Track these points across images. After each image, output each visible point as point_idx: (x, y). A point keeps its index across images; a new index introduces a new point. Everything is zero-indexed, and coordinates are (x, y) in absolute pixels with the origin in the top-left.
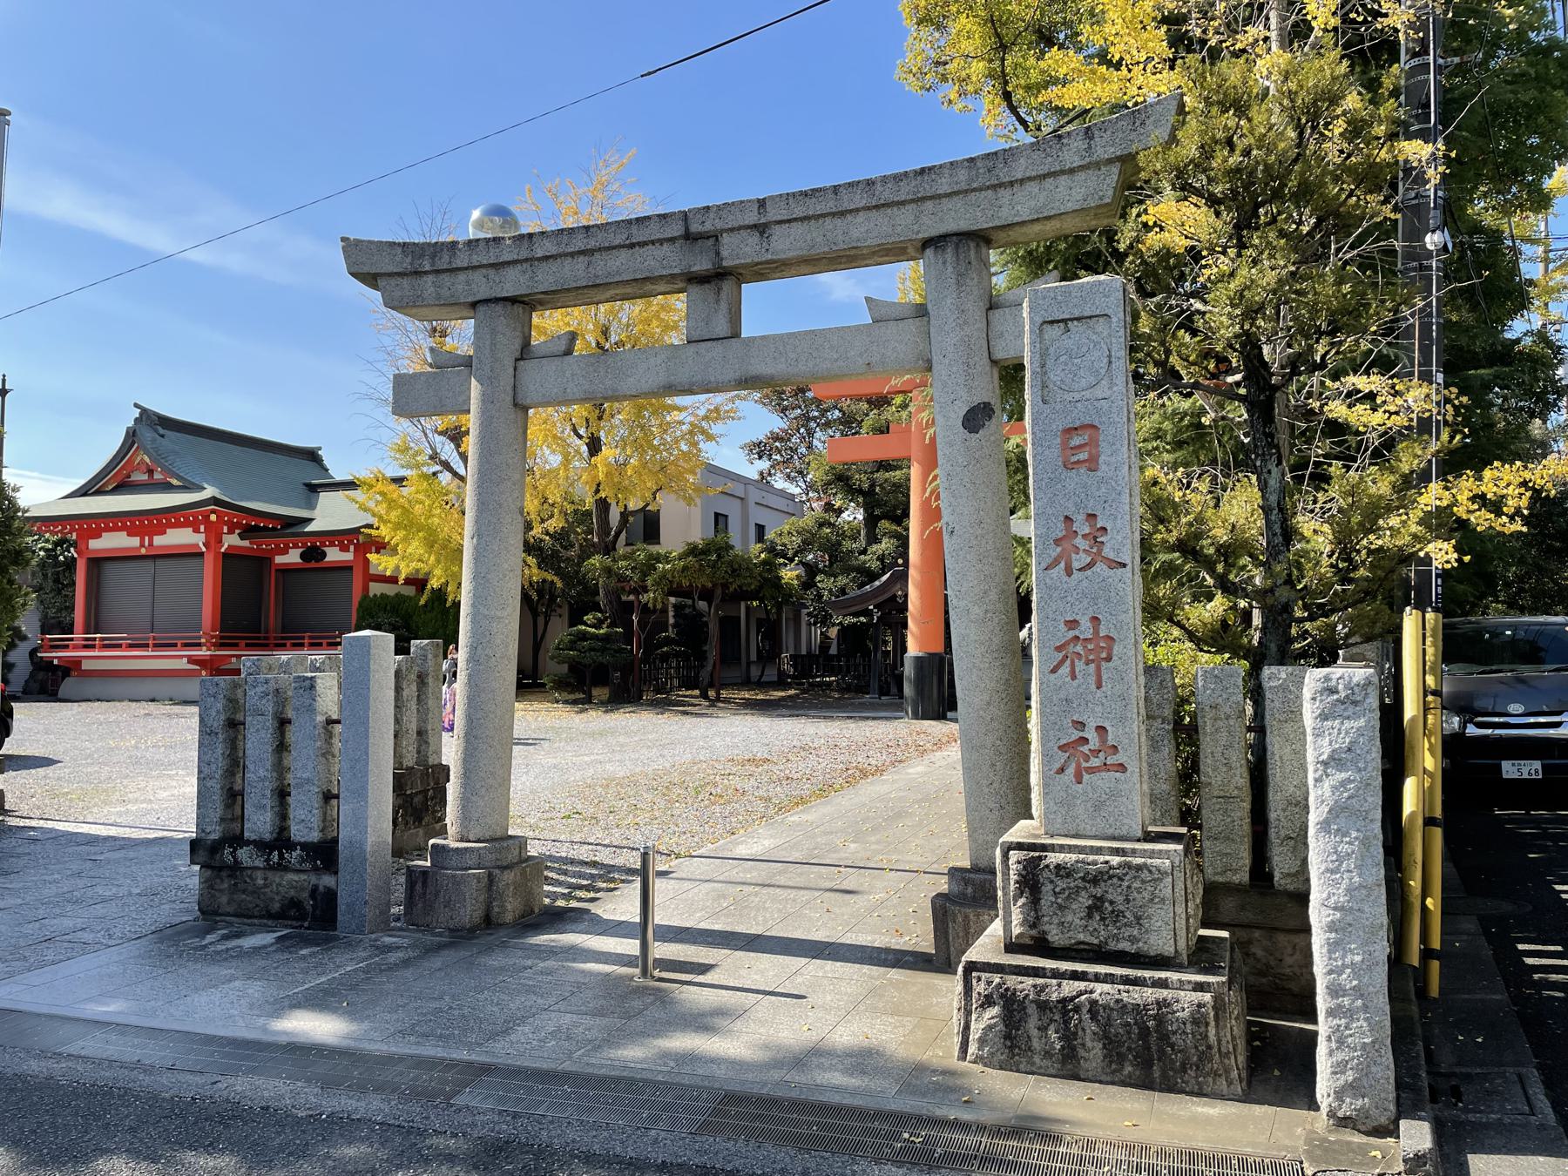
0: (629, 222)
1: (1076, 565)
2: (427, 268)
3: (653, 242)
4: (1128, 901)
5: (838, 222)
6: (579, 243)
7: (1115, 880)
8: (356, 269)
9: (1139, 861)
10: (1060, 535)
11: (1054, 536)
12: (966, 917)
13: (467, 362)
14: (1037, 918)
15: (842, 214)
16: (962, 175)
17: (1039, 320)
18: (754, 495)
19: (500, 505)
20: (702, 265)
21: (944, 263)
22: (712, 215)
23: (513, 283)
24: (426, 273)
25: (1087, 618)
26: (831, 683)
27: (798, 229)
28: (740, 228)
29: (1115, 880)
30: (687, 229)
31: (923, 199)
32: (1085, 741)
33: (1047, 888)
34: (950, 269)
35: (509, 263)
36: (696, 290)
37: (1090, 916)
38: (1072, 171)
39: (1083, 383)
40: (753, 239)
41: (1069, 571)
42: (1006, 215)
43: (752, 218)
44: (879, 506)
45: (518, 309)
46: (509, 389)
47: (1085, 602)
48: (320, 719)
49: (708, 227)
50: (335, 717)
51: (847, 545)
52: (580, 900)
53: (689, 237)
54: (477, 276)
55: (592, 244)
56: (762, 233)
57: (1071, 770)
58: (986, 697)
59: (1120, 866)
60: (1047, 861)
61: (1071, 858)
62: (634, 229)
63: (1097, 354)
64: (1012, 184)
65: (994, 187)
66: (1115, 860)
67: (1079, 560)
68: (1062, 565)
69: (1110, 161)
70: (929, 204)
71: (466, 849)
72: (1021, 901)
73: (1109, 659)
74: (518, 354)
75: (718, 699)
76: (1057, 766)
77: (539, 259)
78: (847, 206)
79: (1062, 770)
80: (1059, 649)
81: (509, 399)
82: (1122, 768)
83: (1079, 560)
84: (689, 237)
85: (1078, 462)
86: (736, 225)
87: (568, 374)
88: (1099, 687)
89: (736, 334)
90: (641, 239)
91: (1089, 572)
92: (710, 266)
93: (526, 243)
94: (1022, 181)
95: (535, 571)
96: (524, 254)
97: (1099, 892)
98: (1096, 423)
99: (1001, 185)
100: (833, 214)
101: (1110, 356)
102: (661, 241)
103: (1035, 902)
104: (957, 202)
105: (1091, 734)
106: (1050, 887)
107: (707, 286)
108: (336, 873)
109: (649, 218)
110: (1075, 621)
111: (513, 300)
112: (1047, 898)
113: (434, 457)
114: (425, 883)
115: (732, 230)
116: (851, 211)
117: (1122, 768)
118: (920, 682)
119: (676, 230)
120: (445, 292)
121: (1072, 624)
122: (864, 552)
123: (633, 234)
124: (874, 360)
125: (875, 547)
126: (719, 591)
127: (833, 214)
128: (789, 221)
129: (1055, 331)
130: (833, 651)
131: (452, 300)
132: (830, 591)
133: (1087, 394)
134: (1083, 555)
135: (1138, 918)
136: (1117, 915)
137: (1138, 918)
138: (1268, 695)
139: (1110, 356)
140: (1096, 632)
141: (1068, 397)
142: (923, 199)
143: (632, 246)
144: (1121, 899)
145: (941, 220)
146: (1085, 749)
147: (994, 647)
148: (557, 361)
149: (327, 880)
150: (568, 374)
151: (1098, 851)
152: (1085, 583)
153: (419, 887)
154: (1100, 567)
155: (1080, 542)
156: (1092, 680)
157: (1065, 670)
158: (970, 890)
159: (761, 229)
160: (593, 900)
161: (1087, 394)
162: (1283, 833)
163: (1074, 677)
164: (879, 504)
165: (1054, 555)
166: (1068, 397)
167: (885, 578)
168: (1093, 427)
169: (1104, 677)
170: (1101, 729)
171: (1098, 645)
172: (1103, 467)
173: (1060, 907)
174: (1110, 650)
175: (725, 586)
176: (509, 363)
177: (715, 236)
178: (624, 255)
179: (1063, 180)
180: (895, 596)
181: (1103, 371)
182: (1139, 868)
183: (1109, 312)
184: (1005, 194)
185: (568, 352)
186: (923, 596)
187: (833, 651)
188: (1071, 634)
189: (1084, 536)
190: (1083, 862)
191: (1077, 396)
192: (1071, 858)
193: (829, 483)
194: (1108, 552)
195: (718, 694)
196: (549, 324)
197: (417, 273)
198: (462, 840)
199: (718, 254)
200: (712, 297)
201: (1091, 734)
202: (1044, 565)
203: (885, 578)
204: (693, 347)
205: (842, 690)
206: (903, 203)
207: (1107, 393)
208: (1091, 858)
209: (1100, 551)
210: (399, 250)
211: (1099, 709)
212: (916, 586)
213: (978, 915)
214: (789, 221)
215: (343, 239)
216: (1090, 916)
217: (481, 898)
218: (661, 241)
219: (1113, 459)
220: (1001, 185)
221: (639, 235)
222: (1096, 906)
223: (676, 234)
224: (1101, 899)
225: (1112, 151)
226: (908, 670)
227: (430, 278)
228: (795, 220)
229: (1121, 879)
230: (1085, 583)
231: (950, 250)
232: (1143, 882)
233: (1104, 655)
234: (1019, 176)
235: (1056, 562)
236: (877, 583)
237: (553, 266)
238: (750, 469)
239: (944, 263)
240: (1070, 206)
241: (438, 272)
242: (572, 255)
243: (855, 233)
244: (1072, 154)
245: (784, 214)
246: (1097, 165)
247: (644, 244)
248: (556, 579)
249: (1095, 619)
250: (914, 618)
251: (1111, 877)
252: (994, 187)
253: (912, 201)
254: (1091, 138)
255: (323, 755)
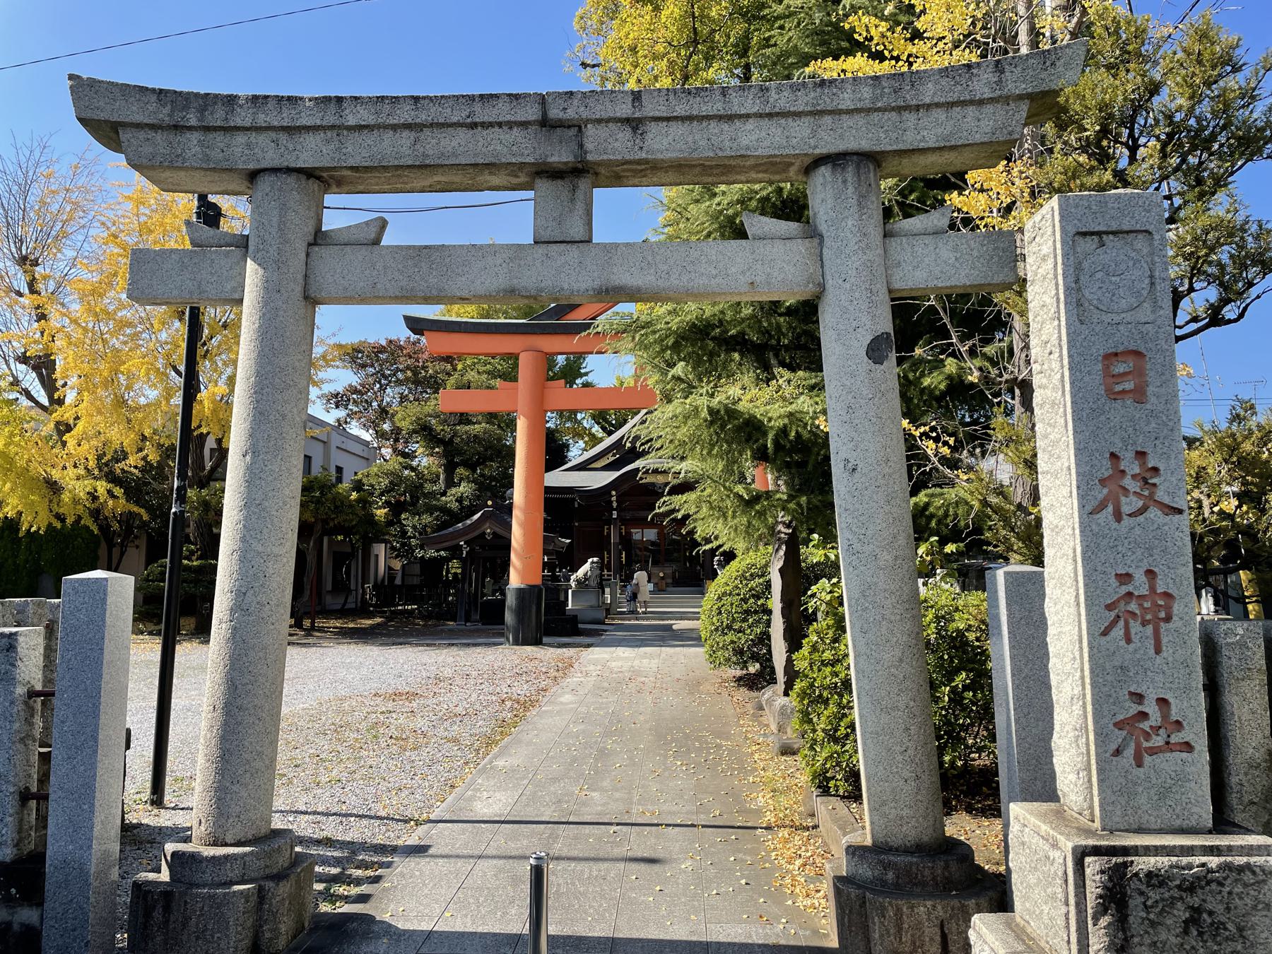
0: (472, 98)
1: (1126, 509)
2: (193, 122)
3: (500, 125)
4: (1228, 909)
5: (725, 127)
6: (405, 114)
7: (1214, 886)
8: (83, 115)
9: (1241, 860)
10: (1106, 474)
11: (1099, 475)
12: (898, 911)
13: (242, 243)
14: (1126, 940)
15: (730, 118)
16: (866, 92)
17: (1072, 230)
18: (336, 440)
19: (284, 417)
20: (561, 155)
21: (845, 182)
22: (575, 102)
23: (311, 151)
24: (190, 128)
25: (1142, 571)
26: (413, 610)
27: (677, 129)
28: (608, 120)
29: (1214, 886)
30: (545, 114)
31: (822, 113)
32: (1144, 716)
33: (1135, 902)
34: (851, 189)
35: (308, 129)
36: (543, 185)
37: (1186, 932)
38: (981, 102)
39: (1123, 304)
40: (624, 134)
41: (1118, 516)
42: (910, 140)
43: (625, 110)
44: (460, 454)
45: (314, 185)
46: (300, 277)
47: (1139, 552)
48: (20, 690)
49: (571, 114)
50: (39, 687)
51: (428, 487)
52: (347, 899)
53: (546, 123)
54: (263, 139)
55: (423, 117)
56: (635, 129)
57: (1130, 752)
58: (898, 653)
59: (1221, 867)
60: (1135, 869)
61: (1163, 862)
62: (477, 107)
63: (1137, 273)
64: (918, 108)
65: (899, 109)
66: (1213, 862)
67: (1135, 503)
68: (1110, 508)
69: (1020, 97)
70: (827, 120)
71: (226, 857)
72: (1105, 921)
73: (1168, 619)
74: (311, 238)
75: (313, 628)
76: (1114, 747)
77: (350, 128)
78: (736, 109)
79: (1117, 752)
80: (1109, 607)
81: (299, 289)
82: (1188, 747)
83: (1130, 504)
84: (546, 123)
85: (1124, 392)
86: (605, 115)
87: (379, 266)
88: (1158, 650)
89: (590, 241)
90: (486, 119)
91: (1141, 518)
92: (571, 159)
93: (333, 107)
94: (928, 107)
95: (122, 501)
96: (331, 119)
97: (1195, 901)
98: (1142, 349)
99: (907, 108)
100: (720, 118)
101: (1151, 277)
102: (511, 125)
103: (1121, 922)
104: (859, 120)
105: (1151, 708)
106: (1141, 899)
107: (560, 182)
108: (40, 904)
109: (496, 96)
110: (1128, 575)
111: (309, 174)
112: (1136, 915)
113: (16, 382)
114: (167, 909)
115: (599, 121)
116: (740, 116)
117: (1188, 747)
118: (521, 611)
119: (532, 113)
120: (216, 154)
121: (1125, 578)
122: (444, 494)
123: (475, 112)
124: (758, 279)
125: (454, 490)
126: (319, 527)
127: (720, 118)
128: (668, 119)
129: (1089, 244)
130: (398, 581)
131: (225, 165)
132: (414, 527)
133: (1128, 317)
134: (1134, 499)
135: (1241, 930)
136: (1219, 927)
137: (1241, 930)
138: (1225, 652)
139: (1151, 277)
140: (1152, 589)
141: (1107, 318)
142: (822, 113)
143: (473, 126)
144: (1220, 908)
145: (841, 136)
146: (1145, 725)
147: (905, 597)
148: (364, 251)
149: (27, 915)
150: (379, 266)
151: (1190, 851)
152: (1138, 531)
153: (158, 914)
154: (1154, 513)
155: (1128, 482)
156: (1150, 644)
157: (1118, 632)
158: (890, 876)
159: (634, 124)
160: (363, 898)
161: (1128, 317)
162: (1246, 799)
163: (1128, 640)
164: (460, 452)
165: (1100, 497)
166: (1107, 318)
167: (476, 517)
168: (1137, 354)
169: (1164, 640)
170: (1163, 702)
171: (1155, 604)
172: (1153, 399)
173: (1153, 924)
174: (1169, 609)
175: (325, 522)
176: (301, 247)
177: (578, 127)
178: (463, 134)
179: (971, 111)
180: (484, 533)
181: (1145, 293)
182: (1241, 869)
183: (1151, 228)
184: (910, 118)
185: (376, 242)
186: (526, 534)
187: (398, 581)
188: (1124, 590)
189: (1134, 477)
190: (1177, 867)
191: (1117, 318)
192: (1163, 862)
193: (415, 432)
194: (1161, 495)
195: (313, 623)
196: (342, 211)
197: (177, 128)
198: (215, 844)
199: (581, 146)
200: (565, 194)
201: (1151, 708)
202: (1089, 508)
203: (476, 517)
204: (542, 249)
205: (427, 617)
206: (797, 115)
207: (1151, 318)
208: (1185, 860)
209: (1151, 496)
210: (154, 98)
211: (1160, 678)
212: (520, 525)
213: (912, 908)
214: (668, 119)
215: (71, 77)
216: (1186, 932)
217: (249, 923)
218: (511, 125)
219: (1163, 390)
220: (907, 108)
221: (483, 114)
222: (1194, 919)
223: (531, 118)
224: (1196, 911)
225: (1022, 88)
226: (511, 600)
227: (194, 137)
228: (676, 118)
229: (1221, 884)
230: (1138, 531)
231: (850, 169)
232: (1246, 885)
233: (1162, 615)
234: (927, 100)
235: (1101, 507)
236: (468, 522)
237: (369, 139)
238: (332, 416)
239: (845, 182)
240: (978, 138)
241: (207, 129)
242: (394, 128)
243: (745, 141)
244: (982, 85)
245: (662, 111)
246: (1006, 99)
247: (491, 125)
248: (142, 511)
249: (1150, 573)
250: (517, 555)
251: (1208, 883)
252: (899, 109)
253: (811, 113)
254: (1002, 72)
255: (22, 740)
